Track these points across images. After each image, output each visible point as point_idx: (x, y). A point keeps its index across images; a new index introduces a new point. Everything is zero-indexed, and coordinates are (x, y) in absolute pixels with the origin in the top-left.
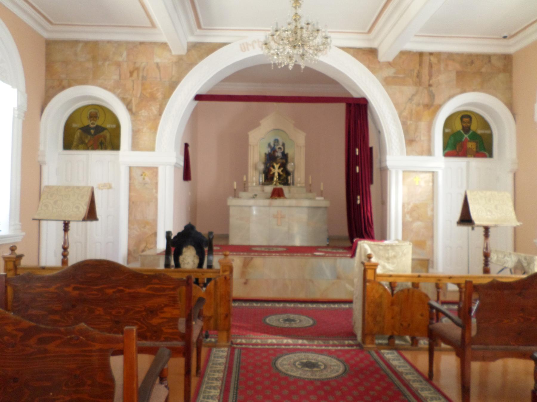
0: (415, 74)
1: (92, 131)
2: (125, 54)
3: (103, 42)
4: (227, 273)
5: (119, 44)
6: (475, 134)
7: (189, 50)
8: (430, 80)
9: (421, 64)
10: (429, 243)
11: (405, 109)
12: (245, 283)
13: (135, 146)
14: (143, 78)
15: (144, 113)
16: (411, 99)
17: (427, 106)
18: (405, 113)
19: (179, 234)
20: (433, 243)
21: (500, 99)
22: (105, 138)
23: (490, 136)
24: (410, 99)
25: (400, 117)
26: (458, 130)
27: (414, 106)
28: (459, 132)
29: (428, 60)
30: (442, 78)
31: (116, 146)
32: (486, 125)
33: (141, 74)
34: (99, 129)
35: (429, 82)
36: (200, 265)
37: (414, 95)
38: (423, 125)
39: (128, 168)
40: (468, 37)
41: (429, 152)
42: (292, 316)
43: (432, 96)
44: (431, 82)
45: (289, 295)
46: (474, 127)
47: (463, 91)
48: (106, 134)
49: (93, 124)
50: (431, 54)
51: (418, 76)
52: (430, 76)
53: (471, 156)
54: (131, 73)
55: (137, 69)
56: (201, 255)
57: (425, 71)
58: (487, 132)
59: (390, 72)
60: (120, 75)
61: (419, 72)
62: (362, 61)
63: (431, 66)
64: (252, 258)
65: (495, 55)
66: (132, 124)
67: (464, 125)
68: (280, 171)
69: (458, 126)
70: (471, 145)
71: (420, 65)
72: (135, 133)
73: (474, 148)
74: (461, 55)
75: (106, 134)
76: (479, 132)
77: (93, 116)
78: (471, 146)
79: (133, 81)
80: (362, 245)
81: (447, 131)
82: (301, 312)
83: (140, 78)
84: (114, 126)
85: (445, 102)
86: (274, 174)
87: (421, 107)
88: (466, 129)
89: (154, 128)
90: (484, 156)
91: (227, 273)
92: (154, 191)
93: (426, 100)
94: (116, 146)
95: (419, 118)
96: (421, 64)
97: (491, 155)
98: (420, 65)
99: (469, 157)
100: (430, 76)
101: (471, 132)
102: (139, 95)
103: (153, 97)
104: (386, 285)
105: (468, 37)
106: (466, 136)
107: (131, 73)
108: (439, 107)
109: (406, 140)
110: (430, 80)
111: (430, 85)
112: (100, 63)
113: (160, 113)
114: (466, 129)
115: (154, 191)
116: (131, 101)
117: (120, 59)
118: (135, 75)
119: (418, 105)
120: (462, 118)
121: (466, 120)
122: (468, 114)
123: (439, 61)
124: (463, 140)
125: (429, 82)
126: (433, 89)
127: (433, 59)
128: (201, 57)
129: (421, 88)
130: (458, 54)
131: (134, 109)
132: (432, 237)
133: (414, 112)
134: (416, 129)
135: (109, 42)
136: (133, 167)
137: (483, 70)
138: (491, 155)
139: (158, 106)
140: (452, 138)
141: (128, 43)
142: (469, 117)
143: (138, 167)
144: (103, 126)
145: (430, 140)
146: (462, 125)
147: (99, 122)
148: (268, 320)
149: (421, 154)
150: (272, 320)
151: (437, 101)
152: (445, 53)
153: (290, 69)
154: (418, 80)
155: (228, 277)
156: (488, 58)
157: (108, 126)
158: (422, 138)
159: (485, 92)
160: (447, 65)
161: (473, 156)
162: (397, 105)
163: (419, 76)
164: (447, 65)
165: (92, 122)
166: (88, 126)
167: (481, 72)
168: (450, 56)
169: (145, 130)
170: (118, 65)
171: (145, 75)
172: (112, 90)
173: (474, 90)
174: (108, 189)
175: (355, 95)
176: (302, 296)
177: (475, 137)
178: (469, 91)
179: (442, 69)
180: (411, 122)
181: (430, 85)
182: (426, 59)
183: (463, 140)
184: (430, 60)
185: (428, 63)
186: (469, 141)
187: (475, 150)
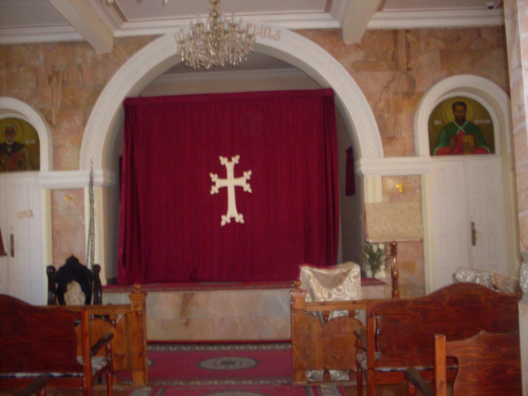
0: (390, 57)
1: (9, 150)
2: (42, 57)
3: (17, 45)
4: (140, 309)
5: (35, 46)
6: (471, 124)
7: (115, 47)
8: (408, 63)
9: (396, 43)
10: (418, 265)
11: (380, 100)
12: (187, 324)
13: (56, 165)
14: (63, 82)
15: (66, 124)
16: (386, 88)
18: (381, 105)
19: (61, 269)
20: (423, 264)
21: (496, 82)
22: (24, 156)
23: (491, 126)
24: (385, 87)
27: (392, 95)
28: (452, 123)
29: (404, 39)
30: (424, 59)
31: (35, 166)
32: (484, 113)
33: (61, 80)
34: (17, 146)
35: (407, 65)
36: (88, 301)
37: (390, 82)
38: (403, 118)
39: (50, 191)
41: (412, 151)
42: (233, 359)
43: (412, 83)
45: (240, 336)
46: (470, 116)
47: (451, 74)
48: (25, 151)
49: (10, 141)
50: (407, 31)
51: (393, 59)
52: (409, 58)
53: (469, 153)
54: (50, 79)
55: (57, 74)
56: (86, 290)
57: (402, 52)
58: (487, 122)
59: (359, 55)
60: (37, 84)
61: (394, 54)
62: (323, 45)
63: (408, 46)
64: (193, 294)
65: (486, 28)
66: (53, 139)
67: (457, 114)
68: (243, 182)
69: (450, 117)
70: (468, 139)
72: (56, 149)
74: (445, 30)
75: (25, 151)
76: (477, 122)
77: (10, 132)
78: (468, 140)
79: (52, 88)
80: (304, 271)
81: (437, 123)
82: (240, 354)
83: (60, 84)
84: (34, 142)
85: (428, 89)
86: (224, 190)
87: (400, 95)
88: (461, 120)
89: (78, 142)
90: (484, 152)
91: (140, 309)
92: (81, 216)
93: (405, 88)
94: (35, 166)
95: (398, 110)
96: (396, 43)
98: (92, 166)
99: (466, 154)
100: (409, 58)
101: (466, 123)
102: (59, 104)
103: (76, 105)
104: (330, 318)
106: (461, 128)
107: (50, 79)
108: (421, 95)
109: (383, 139)
110: (408, 63)
111: (409, 69)
112: (14, 70)
113: (84, 124)
114: (461, 120)
115: (81, 216)
116: (50, 111)
117: (37, 63)
118: (54, 80)
119: (396, 94)
120: (454, 106)
122: (462, 100)
123: (418, 39)
124: (458, 133)
125: (407, 65)
126: (413, 73)
128: (130, 54)
129: (398, 73)
130: (440, 29)
131: (54, 121)
132: (423, 257)
133: (391, 102)
134: (396, 124)
135: (24, 45)
136: (56, 190)
137: (473, 47)
139: (82, 116)
140: (444, 132)
141: (45, 44)
142: (463, 104)
143: (61, 190)
144: (21, 142)
147: (17, 138)
148: (203, 364)
149: (404, 154)
150: (208, 364)
151: (419, 88)
152: (424, 29)
154: (394, 63)
155: (140, 313)
156: (477, 31)
157: (27, 142)
158: (404, 134)
159: (478, 74)
160: (428, 44)
161: (470, 152)
162: (369, 96)
163: (394, 58)
164: (428, 44)
165: (9, 138)
166: (5, 143)
167: (470, 50)
168: (431, 32)
169: (67, 144)
170: (35, 70)
171: (65, 79)
172: (28, 101)
173: (463, 73)
174: (29, 217)
175: (324, 86)
176: (255, 337)
177: (472, 129)
178: (457, 74)
179: (422, 48)
180: (389, 115)
181: (409, 69)
182: (402, 38)
183: (458, 133)
184: (406, 38)
185: (404, 43)
186: (464, 135)
187: (472, 145)
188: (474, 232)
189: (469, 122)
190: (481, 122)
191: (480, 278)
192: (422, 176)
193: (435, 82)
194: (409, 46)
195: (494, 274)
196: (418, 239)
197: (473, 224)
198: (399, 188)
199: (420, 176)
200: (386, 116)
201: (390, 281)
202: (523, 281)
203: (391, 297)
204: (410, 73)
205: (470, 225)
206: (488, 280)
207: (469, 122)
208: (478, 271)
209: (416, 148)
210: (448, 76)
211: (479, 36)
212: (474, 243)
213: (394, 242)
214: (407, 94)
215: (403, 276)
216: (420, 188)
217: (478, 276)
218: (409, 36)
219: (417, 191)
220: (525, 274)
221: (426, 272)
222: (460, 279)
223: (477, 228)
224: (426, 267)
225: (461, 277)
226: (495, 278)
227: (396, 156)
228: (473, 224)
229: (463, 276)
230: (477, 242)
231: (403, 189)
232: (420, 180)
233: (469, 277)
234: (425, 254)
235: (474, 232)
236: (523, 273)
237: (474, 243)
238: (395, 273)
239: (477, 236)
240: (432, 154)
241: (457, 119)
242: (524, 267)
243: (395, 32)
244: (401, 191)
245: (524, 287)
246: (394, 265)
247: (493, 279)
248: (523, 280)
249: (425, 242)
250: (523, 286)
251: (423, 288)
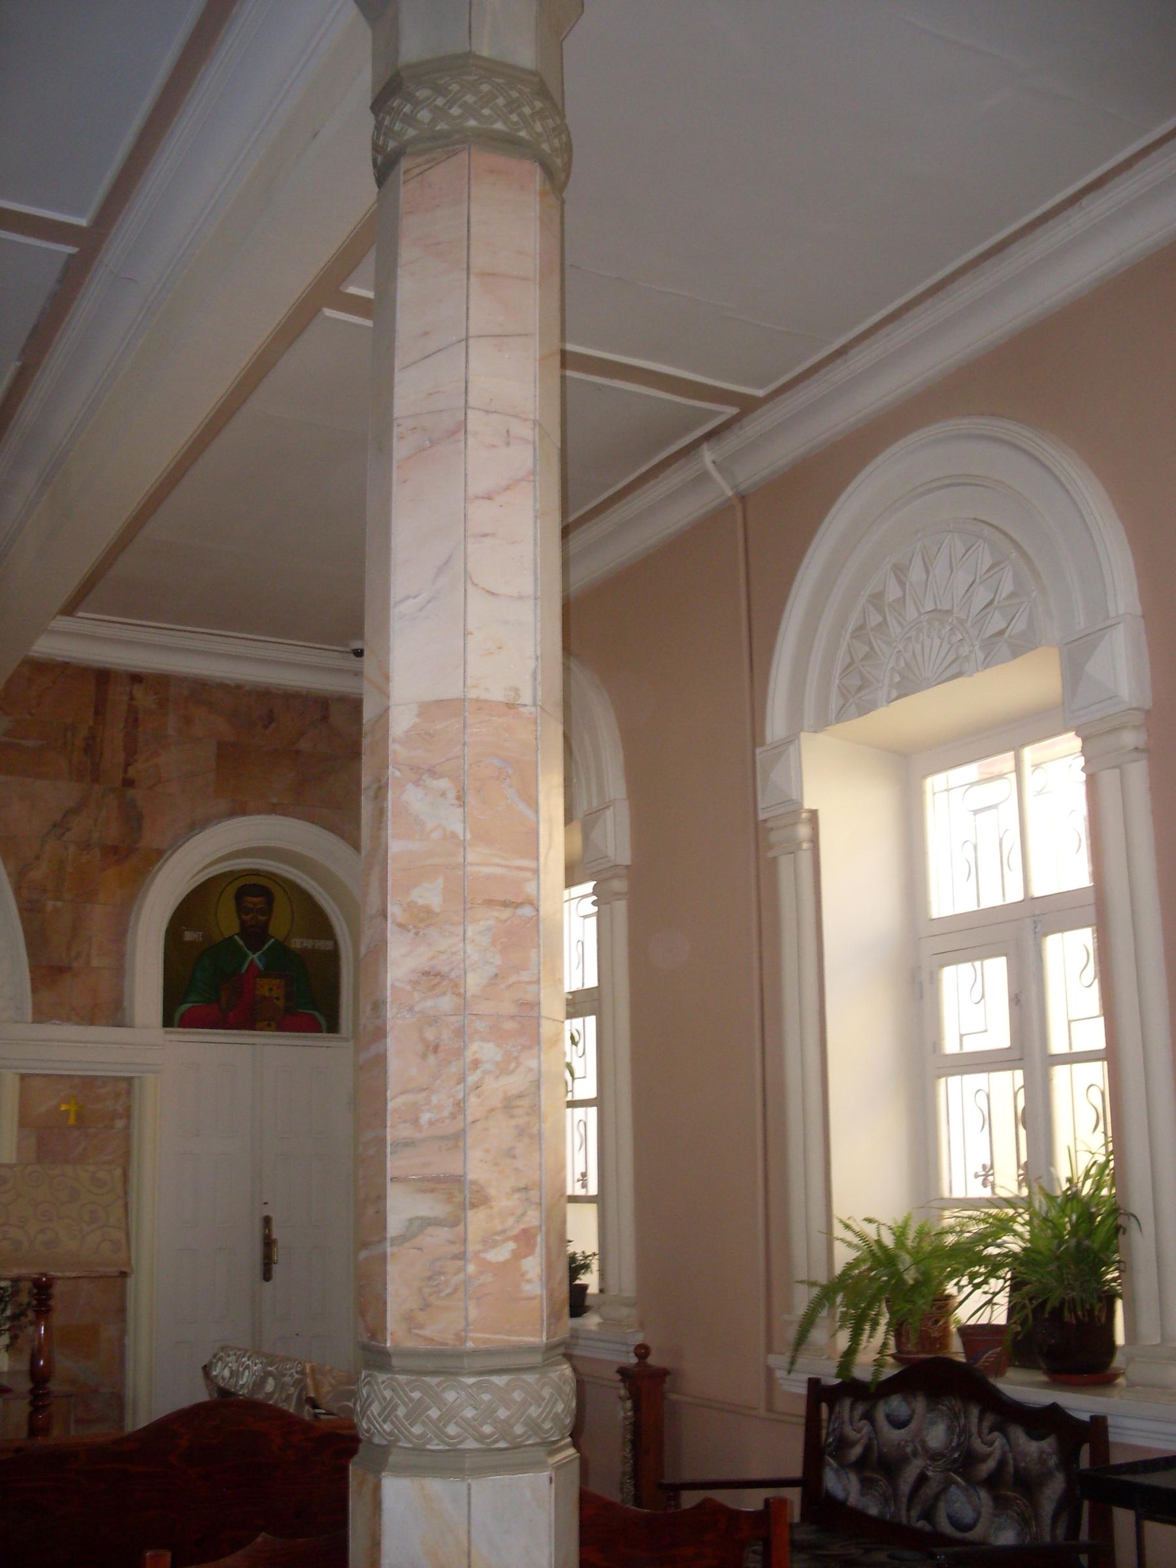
6: (281, 948)
16: (60, 826)
17: (117, 853)
20: (123, 1333)
25: (17, 889)
26: (227, 934)
27: (72, 849)
29: (125, 698)
32: (320, 924)
40: (1128, 164)
43: (133, 819)
44: (132, 772)
46: (279, 927)
47: (239, 810)
50: (136, 678)
51: (88, 749)
52: (131, 750)
53: (268, 1027)
58: (324, 945)
63: (133, 719)
69: (227, 922)
70: (269, 989)
71: (98, 712)
73: (277, 998)
76: (297, 943)
78: (271, 990)
81: (189, 936)
88: (255, 934)
90: (312, 1027)
97: (333, 1026)
98: (98, 712)
100: (131, 750)
105: (1128, 164)
106: (254, 957)
108: (157, 856)
109: (33, 969)
110: (127, 765)
111: (129, 783)
114: (255, 934)
120: (240, 895)
121: (252, 901)
125: (126, 771)
127: (144, 699)
130: (223, 687)
132: (122, 1310)
137: (304, 745)
138: (333, 1026)
142: (264, 892)
145: (120, 969)
146: (240, 918)
149: (91, 1019)
152: (182, 680)
153: (1113, 1507)
158: (95, 963)
163: (91, 747)
167: (298, 752)
173: (273, 809)
178: (259, 812)
180: (59, 904)
181: (129, 783)
184: (132, 698)
187: (280, 1004)
188: (268, 1243)
189: (276, 940)
190: (308, 944)
191: (275, 1379)
192: (136, 1083)
193: (196, 826)
194: (136, 720)
195: (313, 1370)
196: (113, 1270)
197: (267, 1221)
198: (67, 1112)
199: (129, 1080)
200: (50, 905)
201: (24, 1385)
202: (361, 1411)
203: (24, 1433)
204: (130, 793)
205: (258, 1225)
206: (297, 1382)
207: (276, 940)
208: (271, 1359)
209: (126, 1004)
210: (232, 814)
211: (325, 718)
212: (267, 1275)
213: (44, 1275)
214: (115, 850)
215: (65, 1364)
216: (127, 1114)
217: (270, 1374)
218: (139, 692)
219: (120, 1124)
220: (365, 1396)
221: (130, 1354)
222: (223, 1378)
223: (276, 1234)
224: (129, 1340)
225: (227, 1373)
226: (314, 1379)
227: (67, 1019)
228: (267, 1221)
229: (232, 1372)
230: (276, 1269)
231: (80, 1117)
232: (129, 1093)
233: (247, 1373)
234: (130, 1305)
235: (268, 1243)
236: (362, 1393)
237: (267, 1275)
238: (42, 1363)
239: (279, 1254)
240: (168, 1022)
241: (244, 931)
242: (365, 1378)
243: (103, 677)
244: (72, 1121)
245: (363, 1427)
246: (40, 1343)
247: (309, 1381)
248: (362, 1407)
249: (131, 1281)
250: (361, 1425)
251: (118, 1401)
